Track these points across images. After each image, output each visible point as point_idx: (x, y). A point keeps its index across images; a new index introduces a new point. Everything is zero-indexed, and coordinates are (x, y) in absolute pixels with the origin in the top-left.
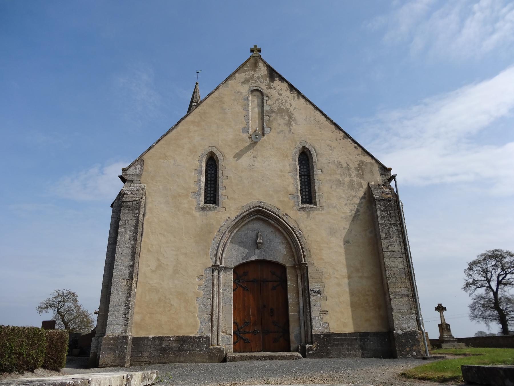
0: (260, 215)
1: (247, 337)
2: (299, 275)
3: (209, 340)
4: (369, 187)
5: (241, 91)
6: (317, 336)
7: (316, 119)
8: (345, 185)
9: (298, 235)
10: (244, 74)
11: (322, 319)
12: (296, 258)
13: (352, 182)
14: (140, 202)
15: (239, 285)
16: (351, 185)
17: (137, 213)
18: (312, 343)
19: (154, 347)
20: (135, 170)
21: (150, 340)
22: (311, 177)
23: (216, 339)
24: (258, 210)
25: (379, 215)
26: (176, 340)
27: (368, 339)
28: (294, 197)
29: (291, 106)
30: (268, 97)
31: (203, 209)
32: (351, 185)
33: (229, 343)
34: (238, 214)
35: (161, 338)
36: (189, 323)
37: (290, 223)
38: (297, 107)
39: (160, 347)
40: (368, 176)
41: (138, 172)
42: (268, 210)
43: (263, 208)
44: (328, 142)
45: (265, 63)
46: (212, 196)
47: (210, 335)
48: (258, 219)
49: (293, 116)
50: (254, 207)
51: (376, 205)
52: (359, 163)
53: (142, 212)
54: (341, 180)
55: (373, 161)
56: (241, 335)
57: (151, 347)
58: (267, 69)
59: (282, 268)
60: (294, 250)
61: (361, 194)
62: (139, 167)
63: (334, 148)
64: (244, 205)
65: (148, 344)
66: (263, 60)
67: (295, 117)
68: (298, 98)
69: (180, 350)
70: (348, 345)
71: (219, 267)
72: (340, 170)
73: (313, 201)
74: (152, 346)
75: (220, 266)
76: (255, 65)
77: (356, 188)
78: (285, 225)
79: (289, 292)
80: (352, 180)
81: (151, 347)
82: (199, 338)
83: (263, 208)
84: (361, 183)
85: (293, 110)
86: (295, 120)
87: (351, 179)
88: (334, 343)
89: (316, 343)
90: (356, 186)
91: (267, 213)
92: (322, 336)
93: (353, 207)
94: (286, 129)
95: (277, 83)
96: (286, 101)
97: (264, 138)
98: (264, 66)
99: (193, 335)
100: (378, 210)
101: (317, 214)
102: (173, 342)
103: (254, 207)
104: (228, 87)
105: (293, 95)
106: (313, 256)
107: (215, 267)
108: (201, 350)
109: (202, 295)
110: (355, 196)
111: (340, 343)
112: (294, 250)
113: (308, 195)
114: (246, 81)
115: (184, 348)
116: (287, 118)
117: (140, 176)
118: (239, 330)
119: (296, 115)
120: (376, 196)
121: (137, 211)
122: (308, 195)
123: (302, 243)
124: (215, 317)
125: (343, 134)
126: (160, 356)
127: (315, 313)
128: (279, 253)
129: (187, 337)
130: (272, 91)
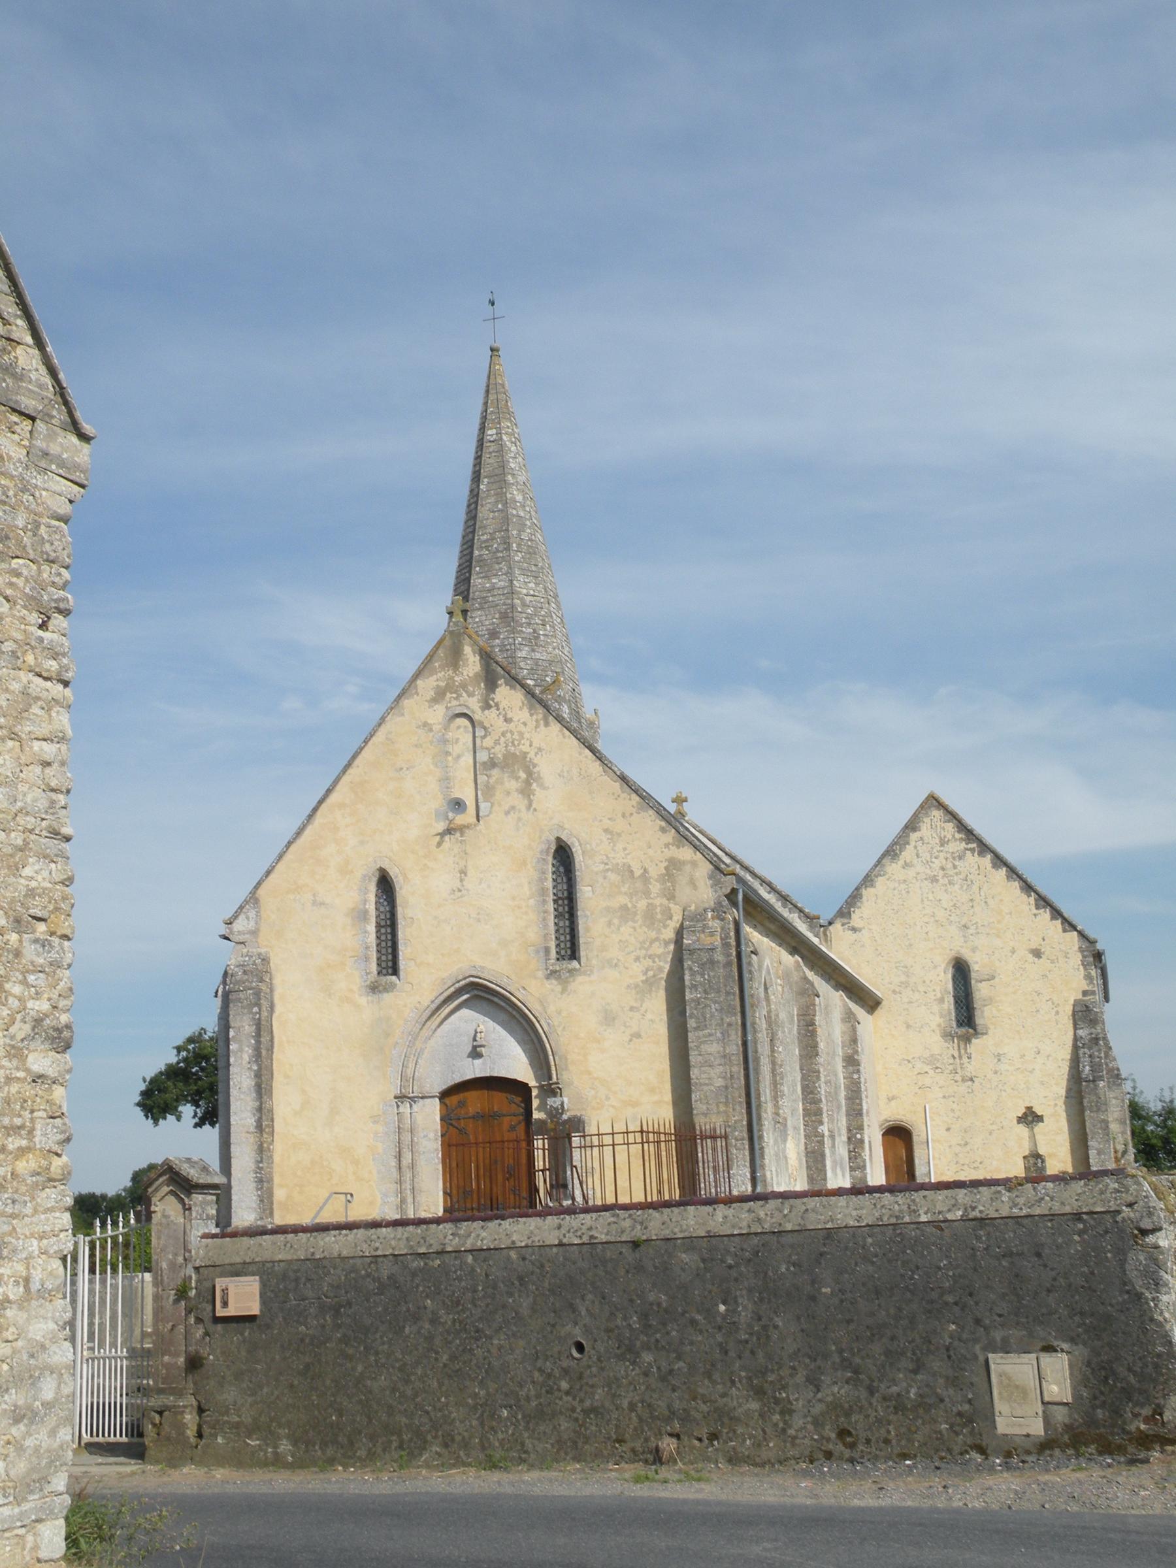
0: (480, 994)
8: (638, 917)
16: (649, 916)
28: (537, 952)
30: (485, 728)
32: (649, 916)
34: (435, 994)
38: (543, 745)
40: (685, 894)
41: (251, 925)
44: (607, 823)
46: (390, 961)
49: (535, 770)
54: (630, 905)
63: (619, 835)
68: (547, 724)
72: (627, 886)
85: (536, 754)
86: (539, 779)
90: (659, 916)
93: (651, 964)
94: (521, 803)
96: (521, 734)
97: (482, 826)
100: (686, 972)
104: (403, 715)
105: (535, 717)
107: (401, 1098)
114: (439, 696)
116: (523, 775)
117: (255, 933)
119: (546, 768)
121: (256, 1009)
125: (638, 798)
128: (515, 1064)
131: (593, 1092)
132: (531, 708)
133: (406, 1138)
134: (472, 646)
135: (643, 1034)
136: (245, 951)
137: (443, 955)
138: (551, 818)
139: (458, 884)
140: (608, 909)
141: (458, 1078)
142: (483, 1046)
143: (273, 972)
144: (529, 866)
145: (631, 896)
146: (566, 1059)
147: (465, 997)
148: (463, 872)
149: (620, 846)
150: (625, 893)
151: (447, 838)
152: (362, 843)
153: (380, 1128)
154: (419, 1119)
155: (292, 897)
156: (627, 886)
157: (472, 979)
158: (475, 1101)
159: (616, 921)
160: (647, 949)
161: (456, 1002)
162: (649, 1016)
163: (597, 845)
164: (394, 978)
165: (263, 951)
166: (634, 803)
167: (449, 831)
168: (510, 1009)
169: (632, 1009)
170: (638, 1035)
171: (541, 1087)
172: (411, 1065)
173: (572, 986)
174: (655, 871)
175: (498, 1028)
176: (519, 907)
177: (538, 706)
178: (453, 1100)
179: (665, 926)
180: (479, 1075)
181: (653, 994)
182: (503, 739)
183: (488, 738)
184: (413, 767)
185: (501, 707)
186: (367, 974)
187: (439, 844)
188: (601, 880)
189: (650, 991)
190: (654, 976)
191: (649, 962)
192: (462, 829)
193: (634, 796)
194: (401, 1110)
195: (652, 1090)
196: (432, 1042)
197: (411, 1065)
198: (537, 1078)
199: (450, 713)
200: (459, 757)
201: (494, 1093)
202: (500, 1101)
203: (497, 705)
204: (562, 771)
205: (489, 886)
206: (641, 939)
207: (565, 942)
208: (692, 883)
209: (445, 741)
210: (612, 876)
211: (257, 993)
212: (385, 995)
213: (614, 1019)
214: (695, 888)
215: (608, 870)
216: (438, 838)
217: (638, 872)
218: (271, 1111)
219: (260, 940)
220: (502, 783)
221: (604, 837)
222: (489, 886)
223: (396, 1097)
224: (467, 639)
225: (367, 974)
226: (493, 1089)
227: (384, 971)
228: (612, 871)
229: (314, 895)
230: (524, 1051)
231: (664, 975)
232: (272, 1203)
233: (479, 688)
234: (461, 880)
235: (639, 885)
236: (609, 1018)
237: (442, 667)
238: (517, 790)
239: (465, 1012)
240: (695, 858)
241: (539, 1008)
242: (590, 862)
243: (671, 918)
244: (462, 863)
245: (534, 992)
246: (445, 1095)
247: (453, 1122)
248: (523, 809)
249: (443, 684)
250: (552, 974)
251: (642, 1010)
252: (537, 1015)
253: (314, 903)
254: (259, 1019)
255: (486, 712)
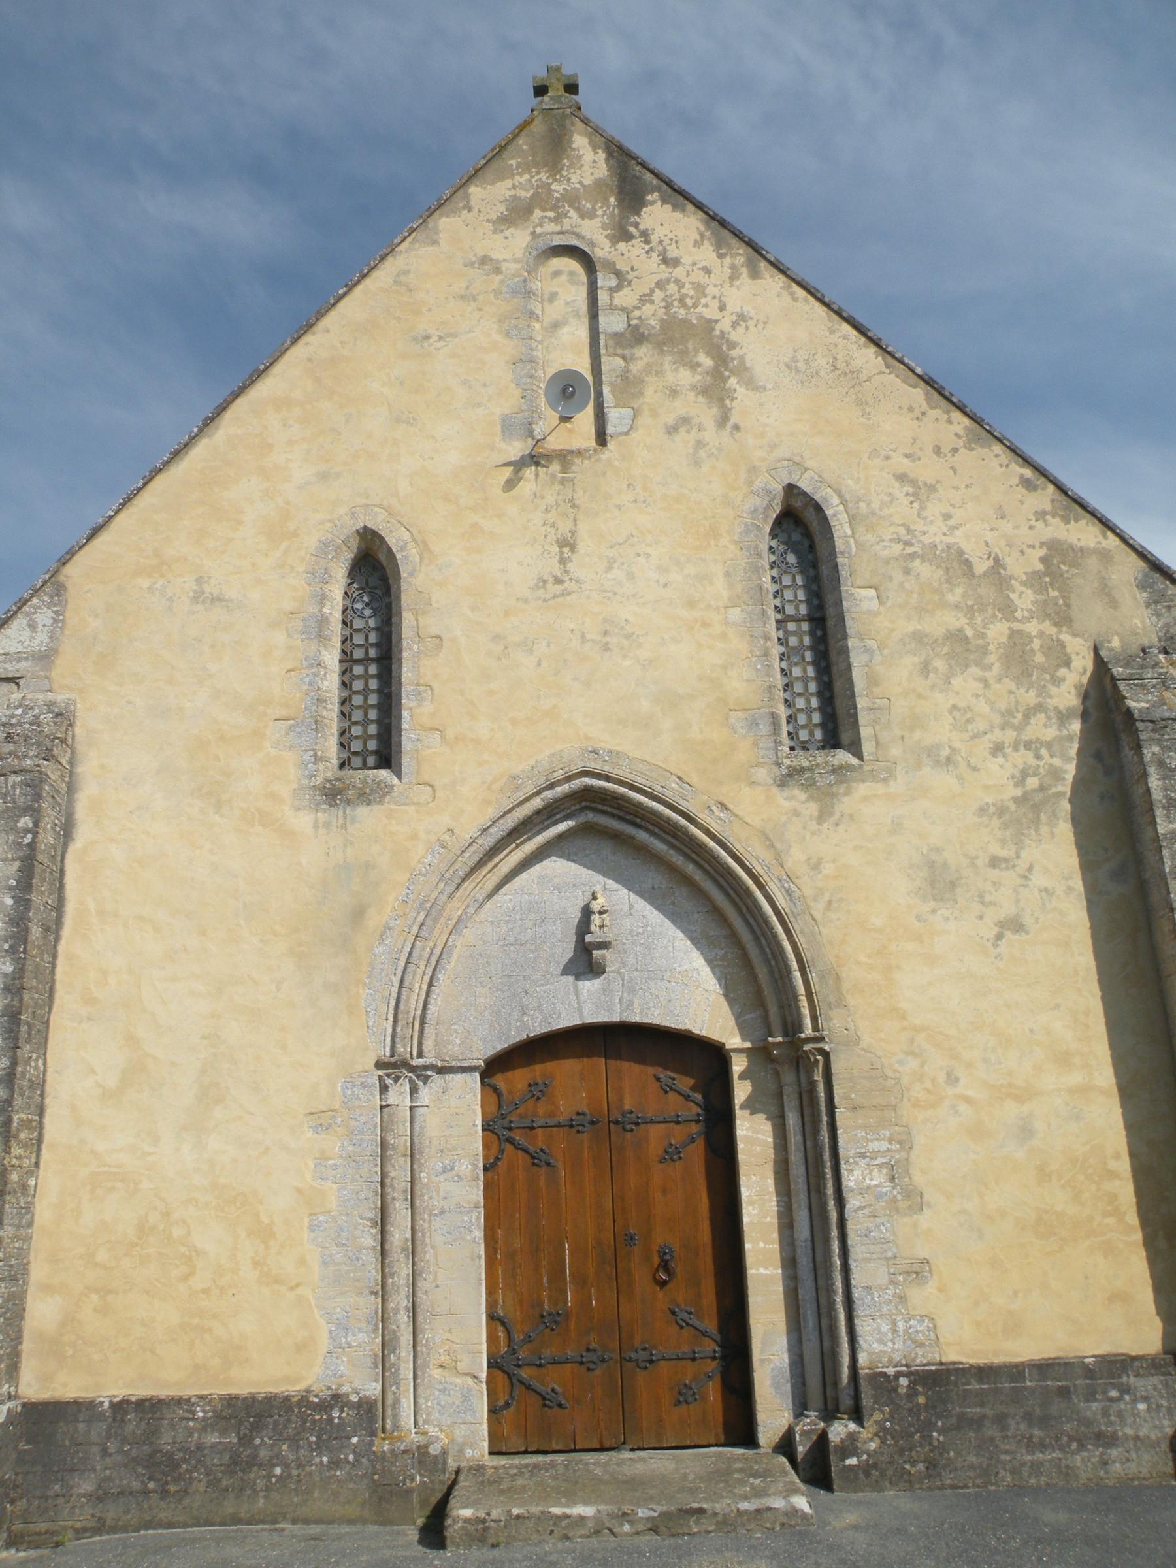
0: (603, 818)
1: (554, 1380)
2: (787, 1090)
3: (369, 1414)
4: (1101, 665)
5: (495, 255)
6: (884, 1383)
7: (841, 364)
8: (992, 658)
9: (781, 902)
10: (508, 183)
11: (902, 1299)
12: (773, 1010)
13: (1017, 639)
14: (42, 778)
15: (510, 1141)
16: (1017, 654)
17: (27, 831)
18: (857, 1415)
19: (120, 1451)
20: (28, 632)
21: (101, 1416)
22: (830, 623)
23: (407, 1404)
24: (587, 791)
25: (1157, 795)
26: (218, 1416)
27: (1125, 1390)
28: (753, 724)
29: (722, 308)
30: (618, 274)
31: (333, 794)
32: (1017, 654)
33: (469, 1418)
34: (491, 812)
35: (150, 1408)
36: (286, 1332)
37: (739, 848)
38: (748, 309)
39: (146, 1449)
40: (1093, 617)
41: (41, 639)
42: (632, 787)
43: (608, 778)
44: (901, 463)
45: (597, 130)
46: (375, 737)
47: (373, 1389)
48: (587, 830)
49: (734, 353)
50: (568, 779)
51: (1138, 748)
52: (1043, 552)
53: (50, 818)
54: (969, 633)
55: (1112, 541)
56: (524, 1373)
57: (105, 1453)
58: (610, 155)
59: (700, 1058)
60: (762, 974)
61: (1067, 693)
62: (44, 617)
63: (932, 488)
64: (519, 768)
65: (94, 1437)
66: (586, 121)
67: (742, 358)
68: (755, 274)
69: (240, 1463)
70: (1028, 1417)
71: (413, 1069)
72: (959, 591)
73: (845, 737)
74: (112, 1447)
75: (416, 1062)
76: (555, 150)
77: (1044, 669)
78: (715, 857)
79: (743, 1170)
80: (1020, 633)
81: (105, 1453)
82: (324, 1406)
83: (608, 778)
84: (1062, 645)
85: (734, 325)
86: (742, 371)
87: (1016, 626)
88: (961, 1417)
89: (877, 1416)
90: (1039, 658)
91: (629, 800)
92: (904, 1381)
93: (1032, 761)
94: (706, 414)
95: (658, 216)
96: (700, 289)
97: (605, 455)
98: (595, 148)
99: (294, 1389)
100: (1152, 770)
101: (866, 799)
102: (206, 1426)
103: (568, 779)
104: (435, 242)
105: (728, 260)
106: (851, 1001)
107: (393, 1067)
108: (335, 1464)
109: (333, 1203)
110: (1040, 708)
111: (988, 1411)
112: (762, 974)
113: (827, 713)
114: (517, 213)
115: (255, 1456)
116: (707, 362)
117: (45, 658)
118: (514, 1352)
119: (752, 348)
120: (1137, 704)
121: (25, 822)
122: (827, 713)
123: (801, 940)
124: (400, 1301)
125: (966, 421)
126: (146, 1492)
127: (868, 1274)
128: (679, 984)
129: (270, 1399)
130: (631, 254)
131: (913, 1064)
132: (718, 244)
133: (399, 1171)
134: (589, 136)
135: (1028, 920)
136: (16, 696)
137: (514, 722)
138: (773, 446)
139: (557, 569)
140: (919, 638)
141: (537, 1027)
142: (605, 945)
143: (80, 748)
144: (725, 540)
145: (970, 612)
146: (838, 978)
147: (563, 827)
148: (567, 544)
149: (934, 509)
150: (957, 606)
151: (529, 472)
152: (324, 477)
153: (334, 1144)
154: (432, 1124)
155: (145, 583)
156: (959, 591)
157: (588, 781)
158: (573, 1084)
159: (940, 664)
160: (1019, 729)
161: (540, 839)
162: (1039, 880)
163: (883, 505)
164: (384, 773)
165: (60, 698)
166: (959, 429)
167: (535, 459)
168: (677, 859)
169: (994, 862)
170: (1015, 925)
171: (760, 1053)
172: (418, 986)
173: (845, 804)
174: (1018, 566)
175: (641, 905)
176: (705, 624)
177: (734, 241)
178: (517, 1080)
179: (1057, 681)
180: (589, 1019)
181: (1044, 829)
182: (658, 295)
183: (626, 291)
184: (454, 335)
185: (654, 238)
186: (317, 759)
187: (510, 485)
188: (898, 576)
189: (1036, 821)
190: (1042, 788)
191: (1023, 758)
192: (565, 458)
193: (957, 415)
194: (392, 1097)
195: (1064, 1060)
196: (468, 935)
197: (418, 986)
198: (744, 1030)
199: (542, 244)
200: (556, 326)
201: (625, 1065)
202: (635, 1083)
203: (645, 235)
204: (795, 359)
205: (631, 577)
206: (1003, 705)
207: (808, 711)
208: (1105, 591)
209: (529, 294)
210: (924, 570)
211: (35, 784)
212: (362, 811)
213: (953, 885)
214: (1114, 604)
215: (912, 556)
216: (508, 472)
217: (981, 567)
218: (39, 1085)
219: (53, 674)
220: (660, 373)
221: (900, 491)
222: (631, 577)
223: (379, 1065)
224: (579, 125)
225: (317, 759)
226: (619, 1057)
227: (357, 761)
228: (923, 558)
229: (199, 580)
230: (710, 962)
231: (1066, 787)
232: (18, 1339)
233: (606, 203)
234: (563, 561)
235: (987, 591)
236: (940, 883)
237: (525, 168)
238: (693, 388)
239: (555, 866)
240: (1105, 543)
241: (766, 856)
242: (869, 537)
243: (1067, 663)
244: (565, 527)
245: (750, 810)
246: (496, 1066)
247: (518, 1137)
248: (709, 423)
249: (526, 194)
250: (791, 777)
251: (1022, 865)
252: (758, 869)
253: (198, 597)
254: (32, 846)
255: (622, 246)
